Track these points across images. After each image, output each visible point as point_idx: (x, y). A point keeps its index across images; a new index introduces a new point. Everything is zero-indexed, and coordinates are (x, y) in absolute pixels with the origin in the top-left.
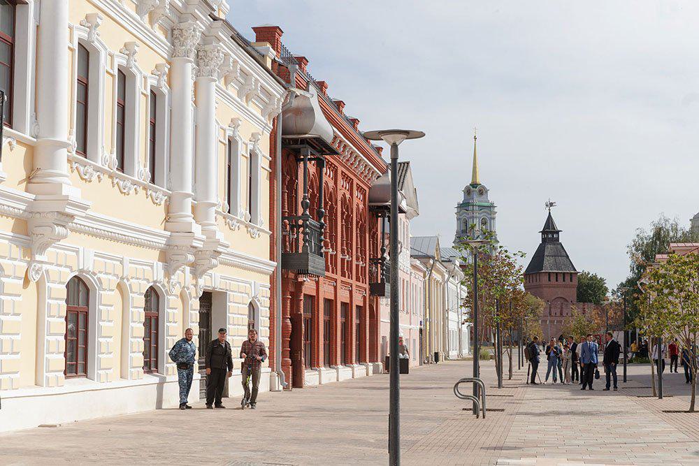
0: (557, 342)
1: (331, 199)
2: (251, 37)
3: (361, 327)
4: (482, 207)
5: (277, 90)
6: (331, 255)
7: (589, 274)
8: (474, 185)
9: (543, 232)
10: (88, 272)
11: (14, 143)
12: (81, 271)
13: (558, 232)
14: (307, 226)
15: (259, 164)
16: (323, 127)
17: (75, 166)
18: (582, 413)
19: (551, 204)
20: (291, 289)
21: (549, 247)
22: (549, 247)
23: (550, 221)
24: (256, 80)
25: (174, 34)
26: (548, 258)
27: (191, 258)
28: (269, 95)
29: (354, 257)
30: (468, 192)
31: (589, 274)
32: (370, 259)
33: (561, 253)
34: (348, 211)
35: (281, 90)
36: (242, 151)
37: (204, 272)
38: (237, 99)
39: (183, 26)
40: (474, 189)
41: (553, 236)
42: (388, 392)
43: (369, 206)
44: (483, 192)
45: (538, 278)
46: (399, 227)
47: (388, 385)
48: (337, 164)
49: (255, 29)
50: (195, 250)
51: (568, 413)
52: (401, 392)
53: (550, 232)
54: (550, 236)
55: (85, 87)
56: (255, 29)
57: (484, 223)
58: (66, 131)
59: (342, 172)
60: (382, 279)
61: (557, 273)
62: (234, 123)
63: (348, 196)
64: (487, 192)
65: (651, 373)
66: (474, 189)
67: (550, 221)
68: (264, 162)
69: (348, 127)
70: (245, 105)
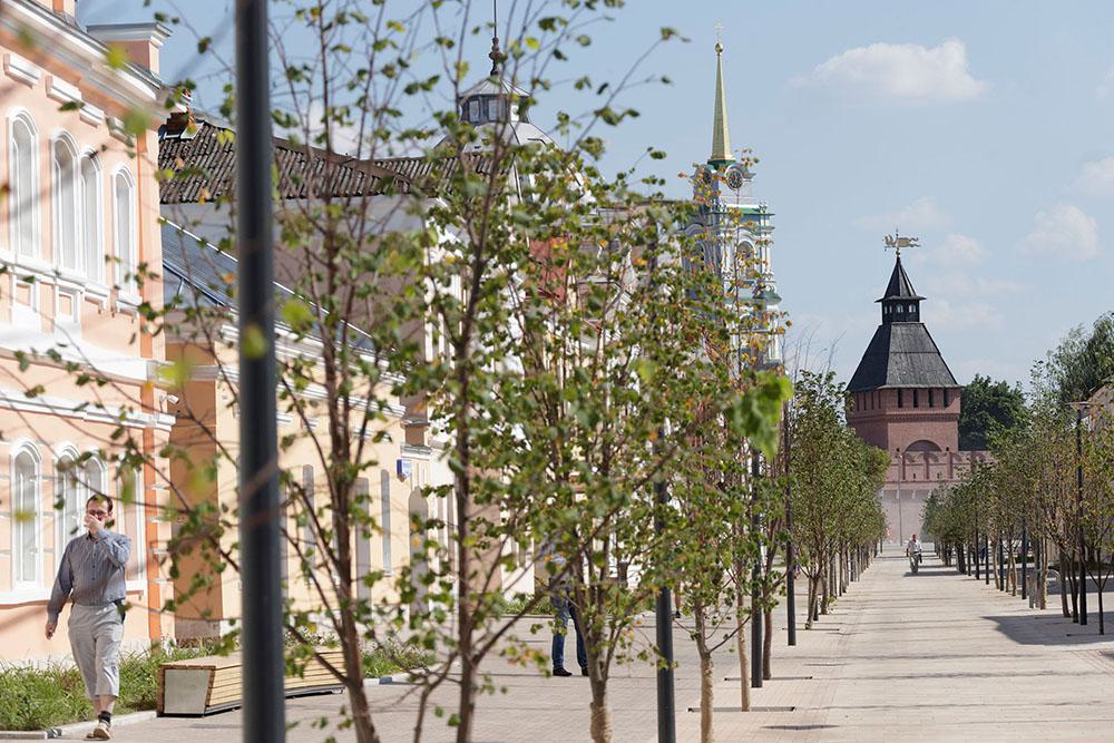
0: (395, 383)
7: (988, 380)
8: (717, 163)
9: (885, 302)
13: (916, 302)
15: (1025, 614)
21: (898, 330)
22: (898, 330)
26: (897, 358)
31: (988, 380)
33: (925, 346)
41: (906, 309)
42: (795, 592)
45: (876, 401)
47: (654, 624)
51: (942, 656)
52: (796, 597)
53: (899, 304)
61: (915, 390)
65: (1098, 611)
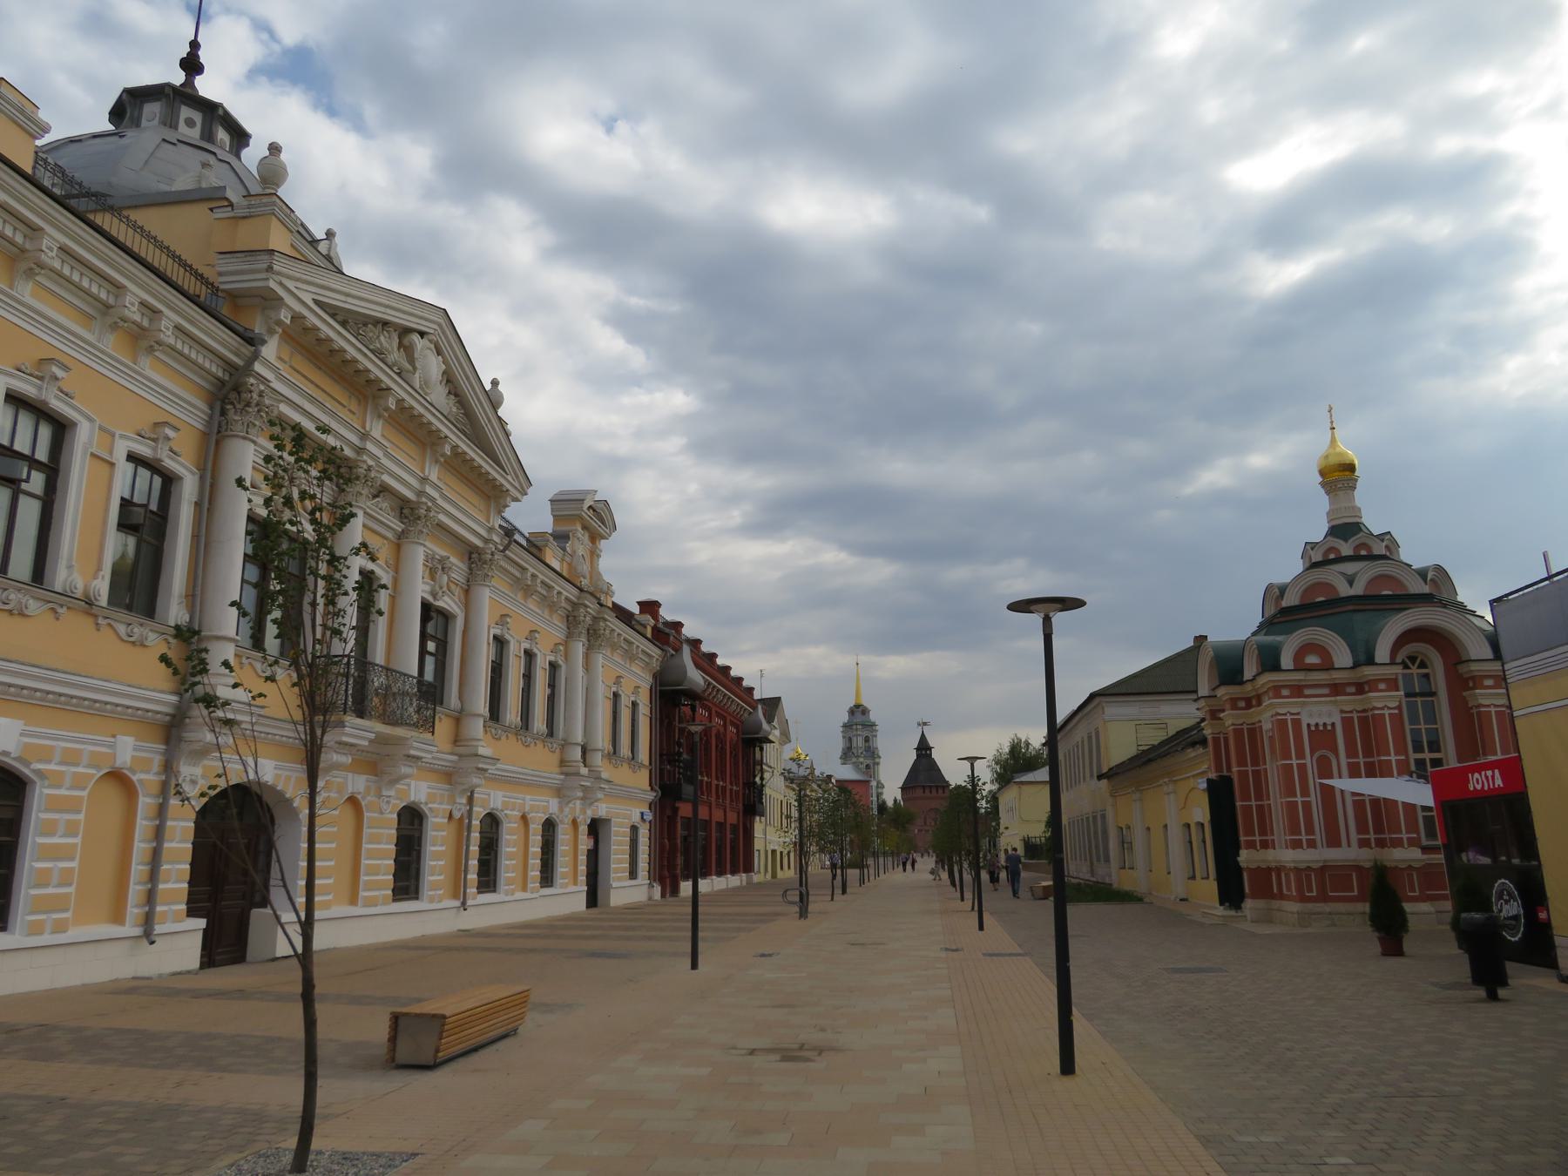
1: (721, 743)
2: (636, 609)
3: (734, 842)
4: (864, 726)
5: (655, 652)
6: (707, 782)
9: (917, 749)
10: (497, 810)
11: (443, 717)
12: (493, 809)
14: (681, 761)
16: (696, 677)
17: (488, 729)
18: (325, 392)
19: (925, 724)
20: (669, 812)
23: (923, 739)
24: (638, 647)
25: (571, 620)
27: (580, 794)
28: (650, 656)
29: (728, 783)
30: (852, 712)
32: (744, 783)
34: (721, 743)
35: (658, 651)
36: (625, 702)
37: (591, 804)
38: (522, 602)
39: (576, 614)
40: (858, 710)
43: (660, 691)
44: (865, 711)
46: (106, 551)
48: (725, 714)
49: (639, 603)
50: (583, 788)
54: (924, 752)
55: (528, 677)
56: (639, 603)
57: (867, 740)
58: (481, 704)
59: (716, 712)
60: (754, 801)
62: (618, 678)
63: (722, 730)
64: (869, 711)
66: (858, 710)
67: (923, 739)
68: (644, 710)
69: (720, 676)
70: (628, 666)
